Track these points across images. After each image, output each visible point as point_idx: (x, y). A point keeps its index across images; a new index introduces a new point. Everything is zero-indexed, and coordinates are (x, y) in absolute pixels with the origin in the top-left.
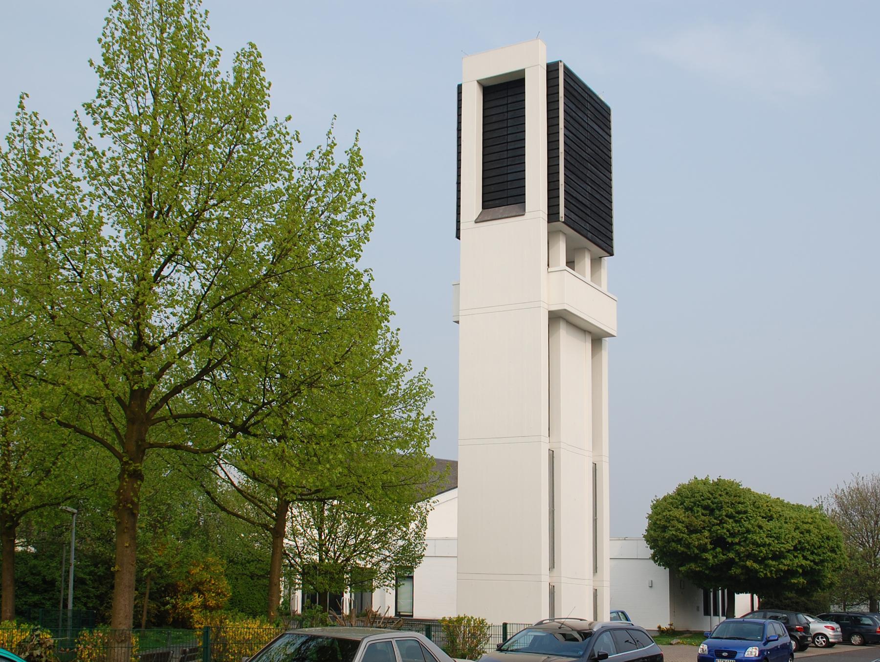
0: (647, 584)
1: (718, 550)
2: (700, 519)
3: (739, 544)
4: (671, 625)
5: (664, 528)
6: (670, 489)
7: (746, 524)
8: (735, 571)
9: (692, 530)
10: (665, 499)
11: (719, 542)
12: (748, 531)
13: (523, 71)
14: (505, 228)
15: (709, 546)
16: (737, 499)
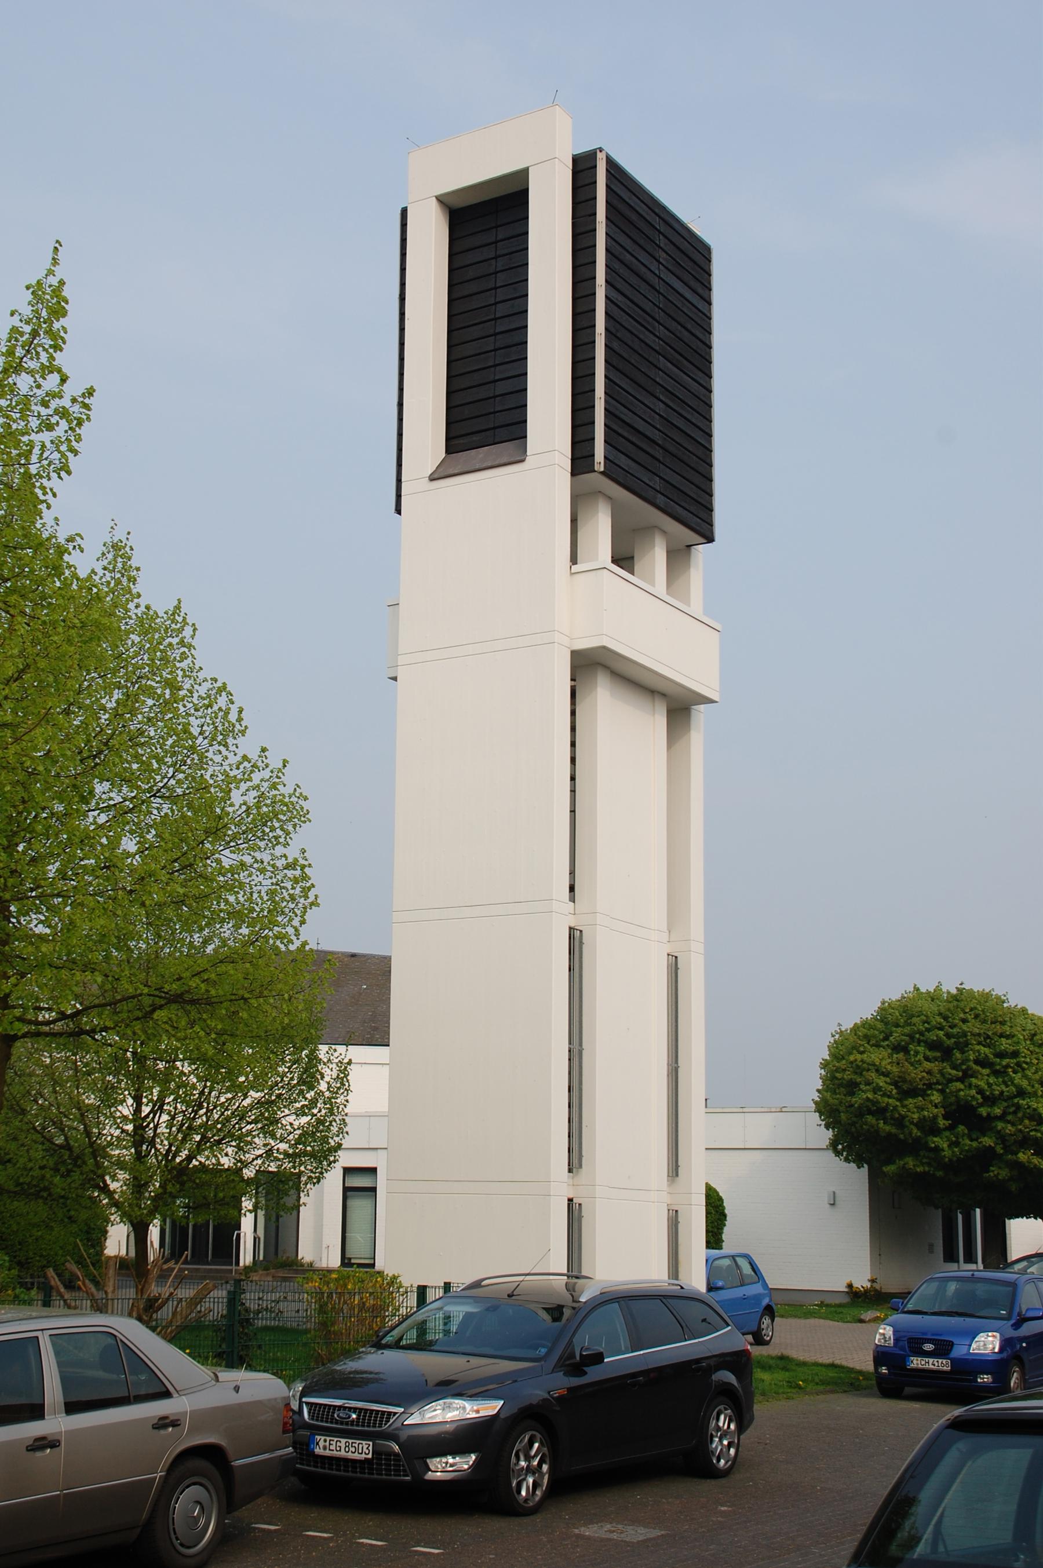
0: (825, 1200)
1: (961, 1128)
2: (922, 1067)
3: (1002, 1118)
4: (873, 1281)
5: (852, 1087)
6: (867, 1010)
7: (1017, 1078)
8: (998, 1172)
9: (907, 1090)
10: (855, 1029)
11: (961, 1114)
12: (1021, 1093)
13: (523, 175)
14: (489, 488)
15: (942, 1123)
16: (998, 1028)
